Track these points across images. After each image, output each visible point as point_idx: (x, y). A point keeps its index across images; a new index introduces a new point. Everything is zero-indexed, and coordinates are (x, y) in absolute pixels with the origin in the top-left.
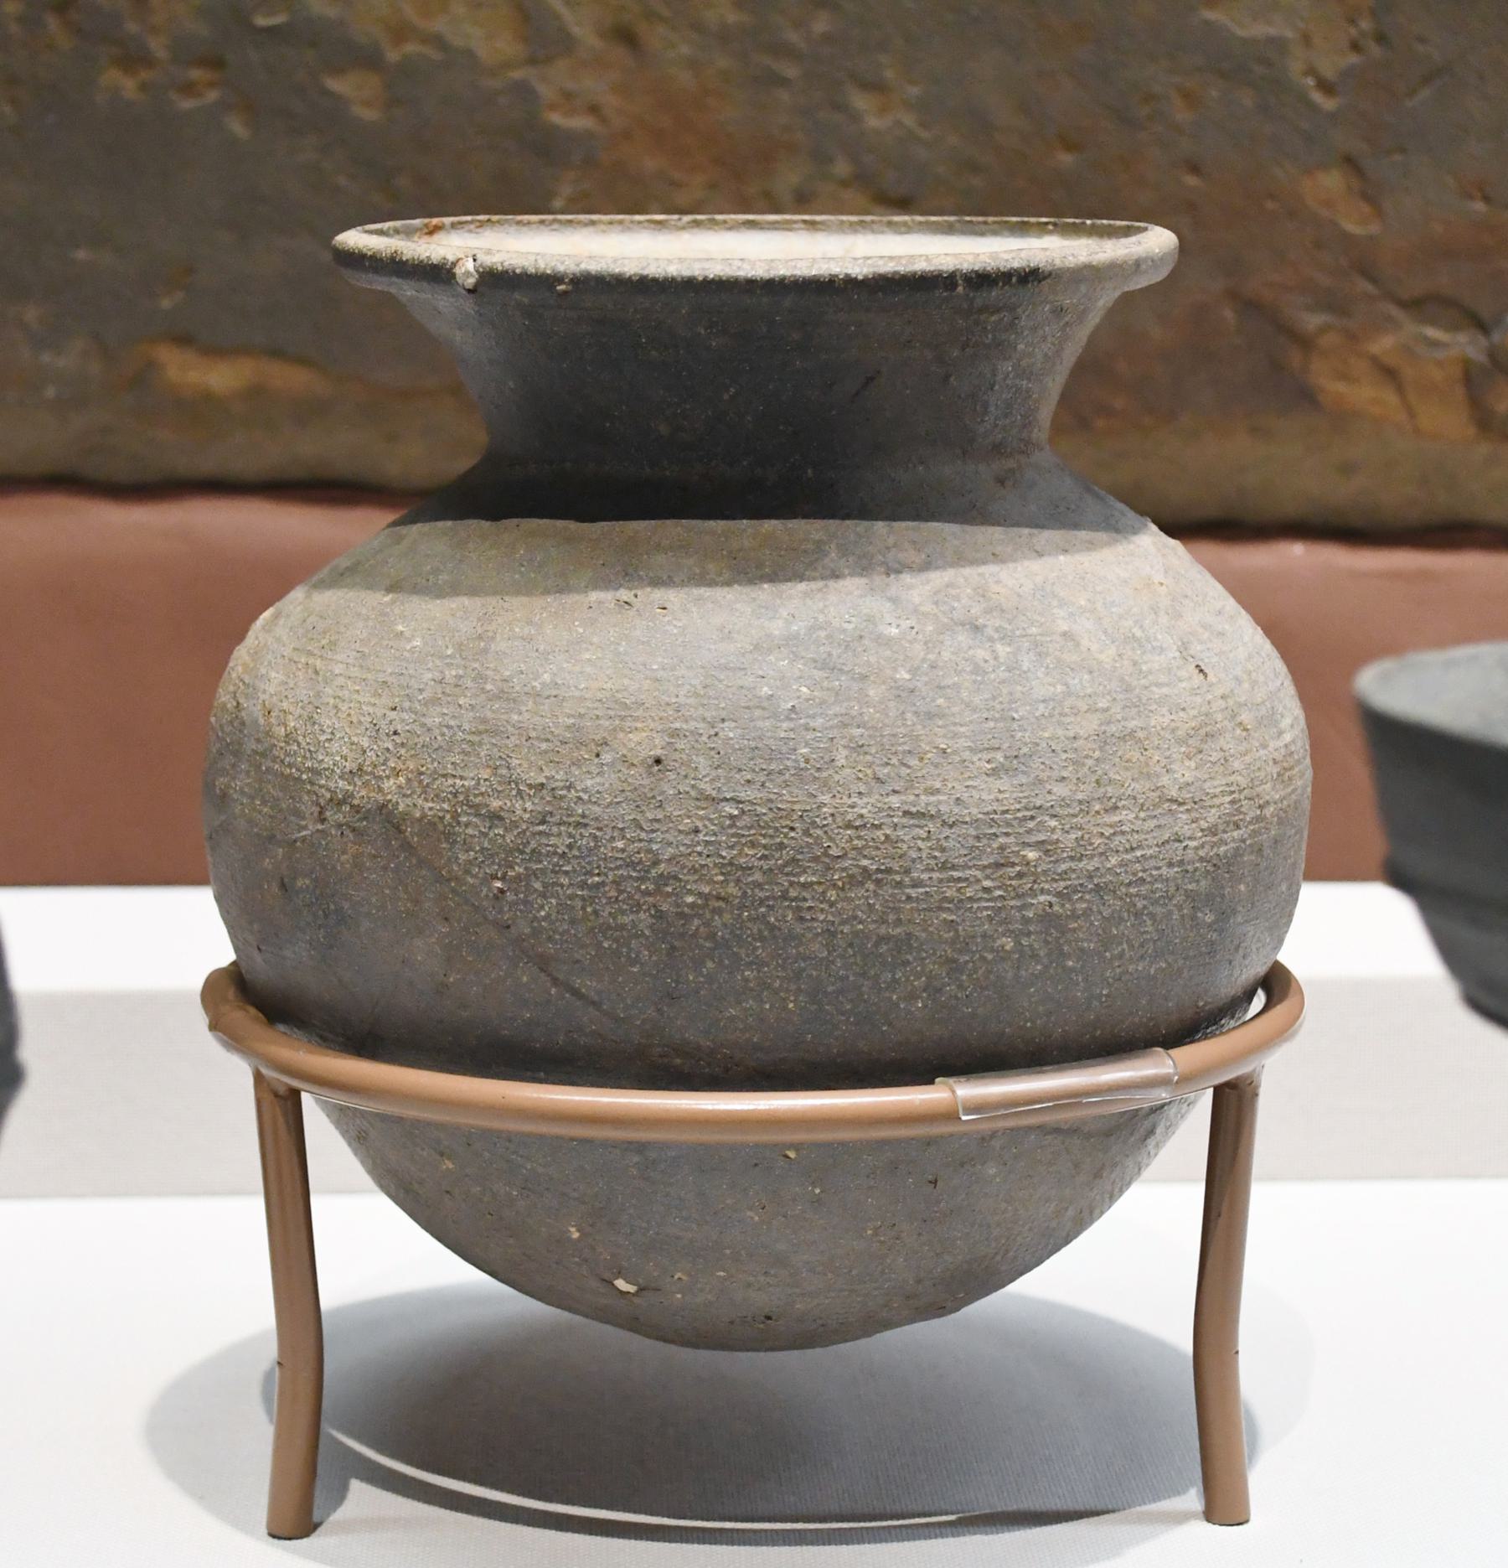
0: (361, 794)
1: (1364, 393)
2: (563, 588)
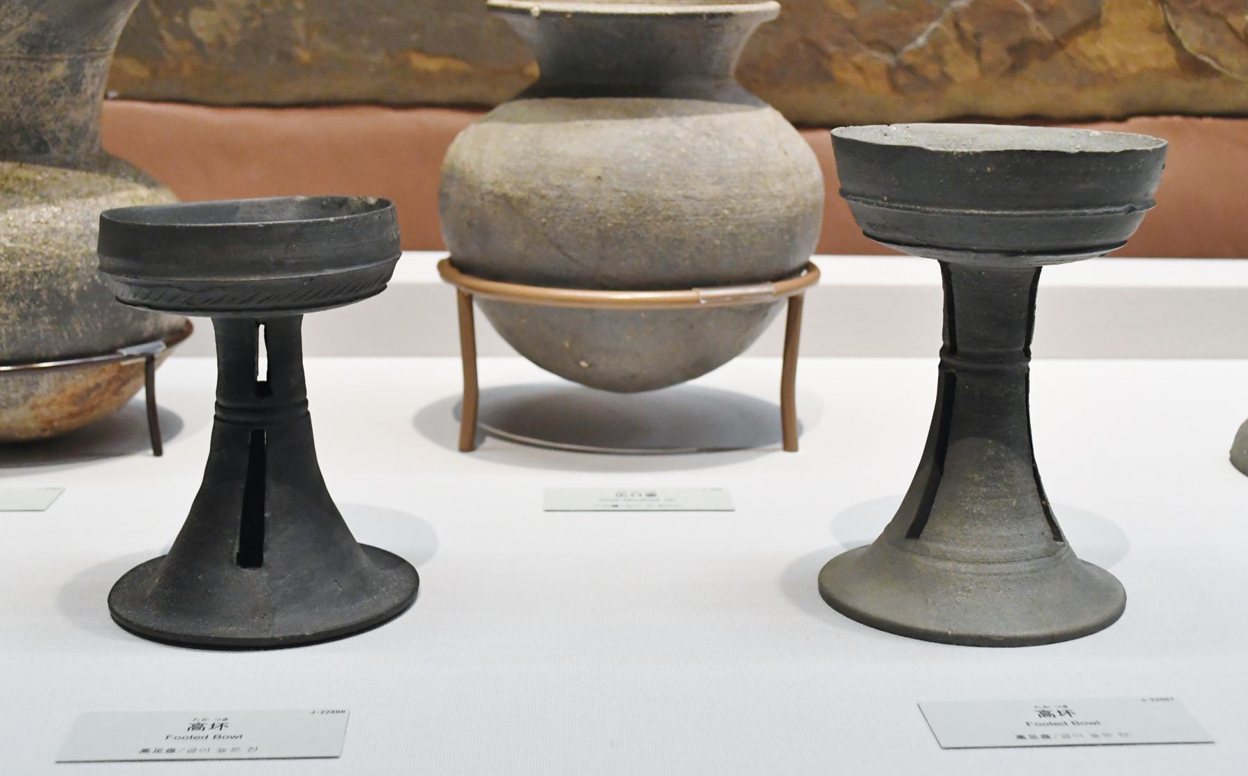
0: (496, 190)
1: (850, 76)
2: (567, 120)
